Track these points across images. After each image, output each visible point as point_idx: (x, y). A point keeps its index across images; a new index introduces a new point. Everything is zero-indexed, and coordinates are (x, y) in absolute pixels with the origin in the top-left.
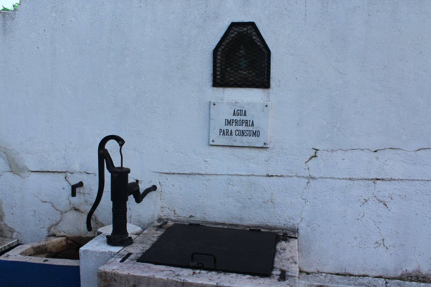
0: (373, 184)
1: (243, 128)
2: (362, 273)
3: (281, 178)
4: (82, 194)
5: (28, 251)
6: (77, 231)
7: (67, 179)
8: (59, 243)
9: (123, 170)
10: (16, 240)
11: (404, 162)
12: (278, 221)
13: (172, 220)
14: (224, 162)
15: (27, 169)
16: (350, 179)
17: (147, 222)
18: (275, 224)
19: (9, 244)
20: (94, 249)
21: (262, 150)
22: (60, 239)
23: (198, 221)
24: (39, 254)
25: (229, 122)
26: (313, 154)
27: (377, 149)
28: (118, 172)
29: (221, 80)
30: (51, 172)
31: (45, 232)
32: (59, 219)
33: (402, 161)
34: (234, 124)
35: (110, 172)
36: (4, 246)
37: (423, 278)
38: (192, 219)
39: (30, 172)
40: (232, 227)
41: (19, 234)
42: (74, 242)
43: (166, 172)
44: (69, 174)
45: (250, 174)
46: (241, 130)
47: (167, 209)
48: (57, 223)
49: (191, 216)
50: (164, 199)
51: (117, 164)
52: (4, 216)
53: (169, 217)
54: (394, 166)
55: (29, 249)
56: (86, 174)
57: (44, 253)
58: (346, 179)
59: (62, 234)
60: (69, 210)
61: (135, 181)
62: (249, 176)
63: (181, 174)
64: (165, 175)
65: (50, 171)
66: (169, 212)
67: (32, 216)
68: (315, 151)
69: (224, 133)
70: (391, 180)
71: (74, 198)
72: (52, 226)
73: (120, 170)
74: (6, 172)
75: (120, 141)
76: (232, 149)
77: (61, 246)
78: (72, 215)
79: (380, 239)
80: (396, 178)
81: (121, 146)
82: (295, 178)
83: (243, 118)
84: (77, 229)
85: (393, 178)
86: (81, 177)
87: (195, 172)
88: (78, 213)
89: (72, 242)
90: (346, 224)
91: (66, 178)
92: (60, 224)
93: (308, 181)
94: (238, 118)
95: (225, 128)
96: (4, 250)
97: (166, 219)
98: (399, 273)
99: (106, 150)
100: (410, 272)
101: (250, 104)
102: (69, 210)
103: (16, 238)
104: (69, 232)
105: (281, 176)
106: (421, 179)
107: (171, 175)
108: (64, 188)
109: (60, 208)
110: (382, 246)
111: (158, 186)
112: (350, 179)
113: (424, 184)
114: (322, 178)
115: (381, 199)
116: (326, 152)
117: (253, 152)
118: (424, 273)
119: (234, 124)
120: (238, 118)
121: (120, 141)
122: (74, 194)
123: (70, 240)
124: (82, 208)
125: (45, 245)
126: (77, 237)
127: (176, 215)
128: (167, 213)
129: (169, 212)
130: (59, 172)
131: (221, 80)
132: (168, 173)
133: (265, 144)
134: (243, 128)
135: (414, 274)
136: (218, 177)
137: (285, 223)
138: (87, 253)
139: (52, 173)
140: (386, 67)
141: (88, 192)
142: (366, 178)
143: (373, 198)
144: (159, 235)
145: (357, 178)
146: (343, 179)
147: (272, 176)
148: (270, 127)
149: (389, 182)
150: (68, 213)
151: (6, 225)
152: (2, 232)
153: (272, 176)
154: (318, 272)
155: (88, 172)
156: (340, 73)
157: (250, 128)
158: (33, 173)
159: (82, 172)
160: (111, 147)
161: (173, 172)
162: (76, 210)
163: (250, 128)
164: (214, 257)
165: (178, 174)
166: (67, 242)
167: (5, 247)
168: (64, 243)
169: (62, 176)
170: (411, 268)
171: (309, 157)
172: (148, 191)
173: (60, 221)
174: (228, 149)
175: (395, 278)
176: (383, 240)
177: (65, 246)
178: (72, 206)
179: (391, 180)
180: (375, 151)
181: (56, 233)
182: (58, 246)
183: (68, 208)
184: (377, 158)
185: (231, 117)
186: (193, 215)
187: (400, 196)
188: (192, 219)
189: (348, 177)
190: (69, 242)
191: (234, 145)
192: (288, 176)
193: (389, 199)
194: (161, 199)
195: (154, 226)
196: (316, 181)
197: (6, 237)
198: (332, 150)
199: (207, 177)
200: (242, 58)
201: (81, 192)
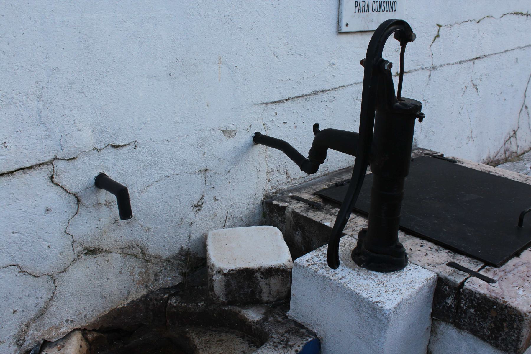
4: (104, 207)
5: (255, 348)
6: (103, 301)
7: (56, 180)
23: (319, 177)
53: (279, 187)
60: (74, 261)
64: (273, 106)
86: (98, 163)
88: (98, 257)
91: (52, 177)
92: (53, 309)
102: (74, 261)
104: (83, 315)
107: (282, 104)
108: (48, 210)
109: (46, 267)
126: (106, 316)
127: (289, 180)
136: (346, 90)
155: (117, 143)
159: (99, 147)
162: (91, 252)
164: (53, 182)
166: (87, 340)
169: (40, 177)
173: (51, 299)
178: (79, 249)
181: (46, 337)
183: (71, 257)
189: (458, 60)
190: (90, 337)
201: (102, 201)
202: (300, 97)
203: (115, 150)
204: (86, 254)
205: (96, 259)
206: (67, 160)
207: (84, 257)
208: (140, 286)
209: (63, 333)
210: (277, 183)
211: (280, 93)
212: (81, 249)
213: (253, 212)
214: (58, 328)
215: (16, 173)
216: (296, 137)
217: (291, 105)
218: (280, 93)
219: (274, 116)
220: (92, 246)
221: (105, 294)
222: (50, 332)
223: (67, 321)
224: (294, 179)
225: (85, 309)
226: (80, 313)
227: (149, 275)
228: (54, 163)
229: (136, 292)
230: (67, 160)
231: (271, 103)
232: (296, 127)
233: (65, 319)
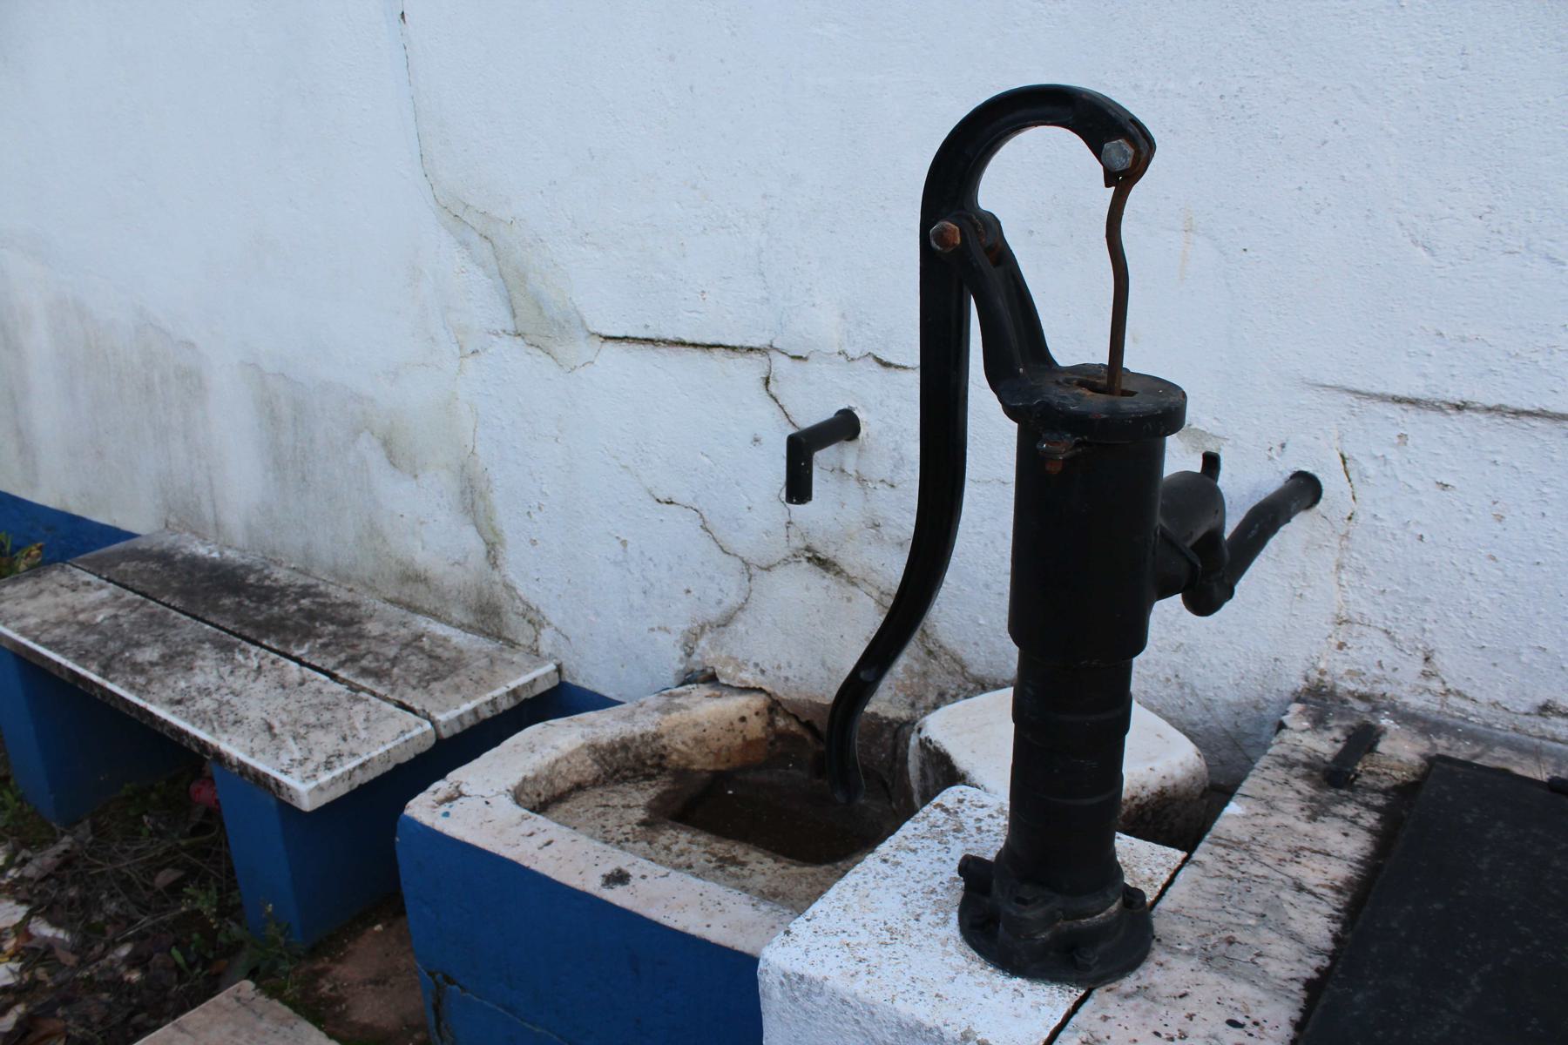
4: (854, 484)
5: (563, 767)
6: (824, 674)
8: (731, 728)
9: (1126, 404)
10: (551, 667)
13: (1407, 718)
15: (583, 323)
17: (1232, 696)
19: (513, 685)
20: (859, 986)
22: (734, 705)
24: (625, 779)
28: (1078, 423)
30: (695, 345)
31: (672, 661)
32: (733, 599)
35: (1011, 412)
36: (489, 696)
39: (598, 341)
41: (562, 640)
42: (808, 725)
43: (1402, 392)
44: (781, 364)
48: (726, 621)
49: (1545, 709)
50: (1361, 572)
51: (1074, 338)
52: (502, 544)
55: (572, 754)
56: (876, 366)
57: (649, 777)
59: (749, 677)
60: (786, 561)
63: (1517, 413)
64: (1394, 411)
65: (688, 339)
66: (1388, 655)
67: (615, 563)
71: (797, 509)
72: (702, 628)
73: (1095, 403)
74: (497, 334)
75: (1116, 139)
77: (739, 741)
78: (798, 588)
81: (1121, 180)
84: (823, 664)
89: (794, 728)
96: (489, 715)
97: (1363, 698)
99: (991, 224)
102: (786, 561)
103: (550, 657)
104: (783, 673)
107: (1434, 416)
109: (742, 543)
111: (1332, 483)
121: (1116, 139)
122: (798, 488)
123: (787, 714)
124: (848, 559)
125: (657, 736)
127: (1435, 685)
128: (1372, 663)
129: (1388, 655)
130: (734, 348)
132: (1414, 402)
138: (808, 994)
139: (697, 353)
141: (886, 475)
144: (1340, 872)
150: (779, 572)
151: (509, 588)
152: (498, 614)
155: (886, 358)
158: (610, 343)
159: (851, 352)
160: (1038, 190)
161: (1455, 396)
162: (822, 563)
165: (1498, 410)
166: (771, 723)
167: (494, 702)
168: (756, 728)
169: (748, 371)
172: (1268, 517)
177: (758, 741)
178: (797, 543)
181: (718, 668)
182: (723, 742)
190: (781, 723)
194: (1340, 566)
195: (1288, 764)
197: (512, 644)
201: (850, 469)
202: (1530, 414)
203: (882, 370)
204: (809, 559)
205: (826, 582)
206: (793, 357)
207: (805, 564)
208: (901, 695)
209: (742, 681)
210: (1376, 671)
211: (1425, 376)
212: (802, 545)
213: (1255, 707)
214: (740, 667)
215: (716, 351)
216: (1494, 552)
217: (1483, 433)
218: (1425, 376)
219: (1396, 446)
220: (826, 552)
221: (829, 663)
222: (726, 664)
223: (756, 665)
224: (1459, 694)
225: (790, 666)
226: (779, 667)
227: (926, 686)
228: (772, 354)
229: (890, 701)
230: (793, 357)
231: (1383, 398)
232: (1500, 518)
233: (755, 659)
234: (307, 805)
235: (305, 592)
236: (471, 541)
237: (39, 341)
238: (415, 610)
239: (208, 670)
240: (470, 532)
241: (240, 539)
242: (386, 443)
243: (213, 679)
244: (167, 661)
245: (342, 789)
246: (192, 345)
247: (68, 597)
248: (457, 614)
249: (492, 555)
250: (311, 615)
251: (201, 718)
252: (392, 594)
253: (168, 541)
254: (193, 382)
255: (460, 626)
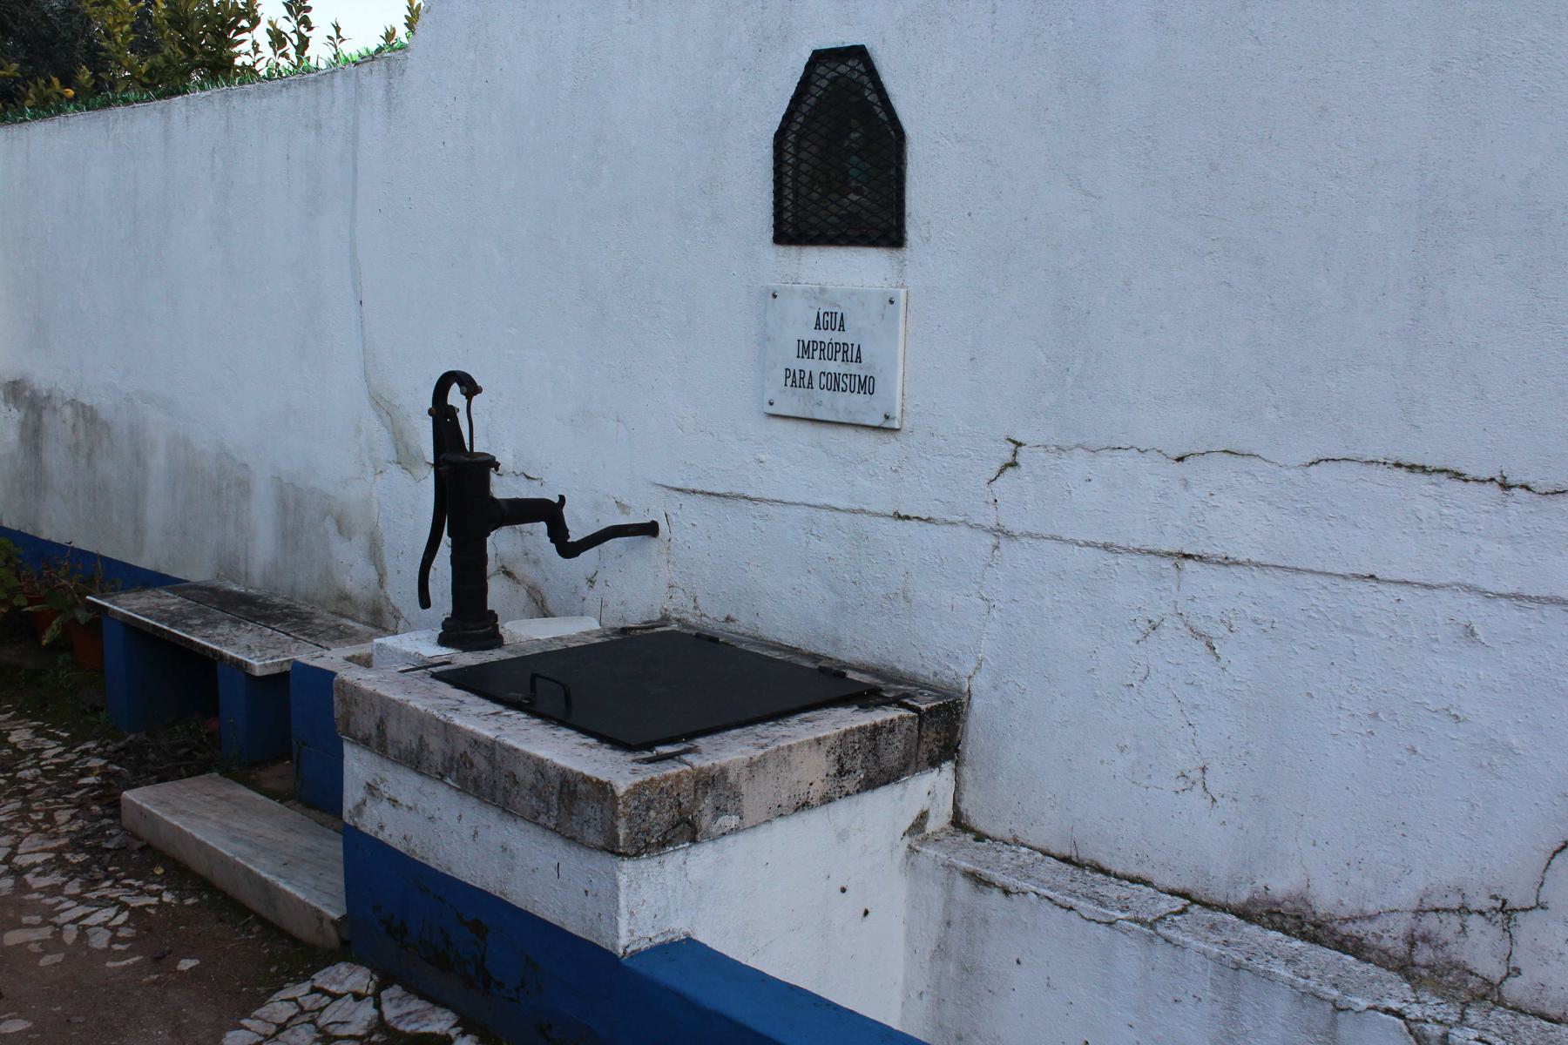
0: (1174, 571)
1: (834, 367)
2: (1135, 871)
3: (929, 526)
11: (1270, 504)
12: (919, 662)
14: (801, 466)
16: (1106, 547)
18: (912, 669)
21: (886, 436)
25: (806, 349)
26: (1008, 457)
27: (1184, 451)
29: (797, 223)
33: (1262, 498)
34: (817, 354)
37: (1317, 926)
38: (731, 626)
40: (795, 659)
45: (856, 506)
46: (830, 373)
47: (680, 593)
54: (1237, 515)
58: (1094, 545)
61: (556, 500)
62: (853, 512)
64: (677, 494)
68: (1013, 446)
69: (796, 379)
70: (1227, 562)
76: (817, 428)
79: (1194, 765)
80: (1242, 559)
82: (963, 530)
83: (837, 337)
85: (1231, 555)
87: (736, 491)
90: (1096, 696)
93: (994, 541)
94: (825, 336)
95: (797, 365)
98: (1243, 895)
100: (1279, 898)
101: (853, 294)
105: (929, 520)
106: (1321, 569)
110: (1198, 789)
111: (663, 526)
112: (1106, 547)
113: (1334, 589)
114: (1030, 535)
115: (1200, 625)
116: (1041, 453)
117: (864, 443)
118: (1321, 911)
119: (817, 354)
120: (825, 336)
121: (471, 388)
124: (518, 572)
130: (724, 496)
131: (797, 223)
133: (887, 417)
134: (834, 367)
135: (1288, 905)
137: (937, 668)
140: (1214, 167)
142: (1151, 548)
143: (1176, 619)
145: (1124, 544)
146: (1087, 544)
147: (908, 518)
148: (904, 366)
149: (1223, 568)
151: (387, 599)
153: (908, 518)
154: (1016, 841)
156: (1087, 193)
157: (853, 368)
160: (455, 397)
161: (692, 486)
163: (853, 368)
170: (1281, 885)
171: (997, 466)
174: (807, 431)
175: (1223, 908)
176: (1204, 769)
179: (1227, 562)
180: (1181, 459)
184: (1186, 484)
185: (811, 335)
186: (734, 615)
187: (1255, 621)
188: (731, 626)
191: (817, 417)
192: (946, 522)
193: (1224, 628)
196: (1017, 544)
198: (1058, 448)
199: (763, 507)
200: (840, 160)
220: (510, 568)
234: (258, 672)
235: (288, 607)
236: (372, 574)
237: (158, 461)
238: (342, 615)
239: (225, 629)
240: (372, 569)
241: (258, 582)
242: (339, 522)
243: (226, 631)
244: (205, 625)
245: (276, 670)
246: (246, 466)
247: (156, 600)
248: (363, 617)
249: (381, 584)
250: (286, 615)
251: (217, 643)
252: (333, 608)
253: (217, 583)
254: (244, 487)
255: (364, 623)
